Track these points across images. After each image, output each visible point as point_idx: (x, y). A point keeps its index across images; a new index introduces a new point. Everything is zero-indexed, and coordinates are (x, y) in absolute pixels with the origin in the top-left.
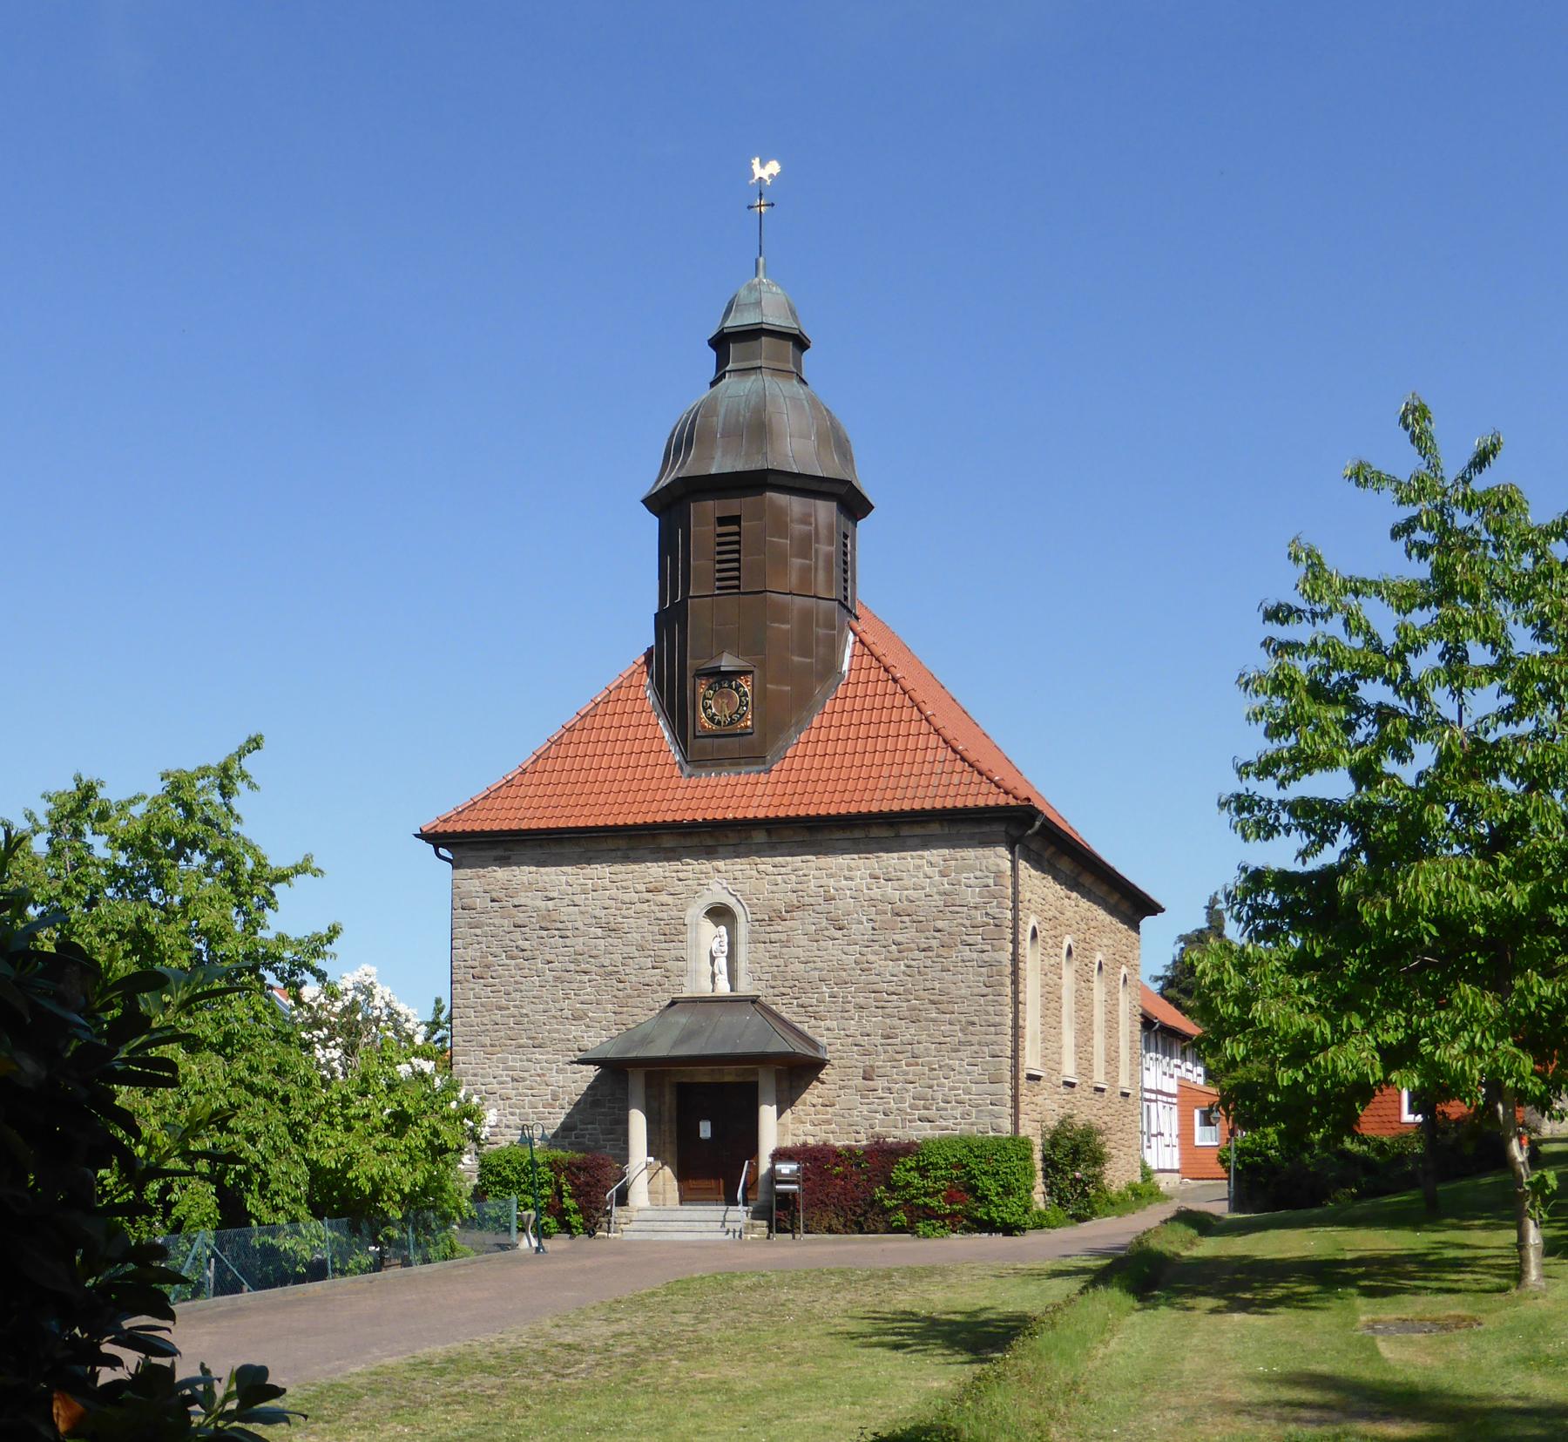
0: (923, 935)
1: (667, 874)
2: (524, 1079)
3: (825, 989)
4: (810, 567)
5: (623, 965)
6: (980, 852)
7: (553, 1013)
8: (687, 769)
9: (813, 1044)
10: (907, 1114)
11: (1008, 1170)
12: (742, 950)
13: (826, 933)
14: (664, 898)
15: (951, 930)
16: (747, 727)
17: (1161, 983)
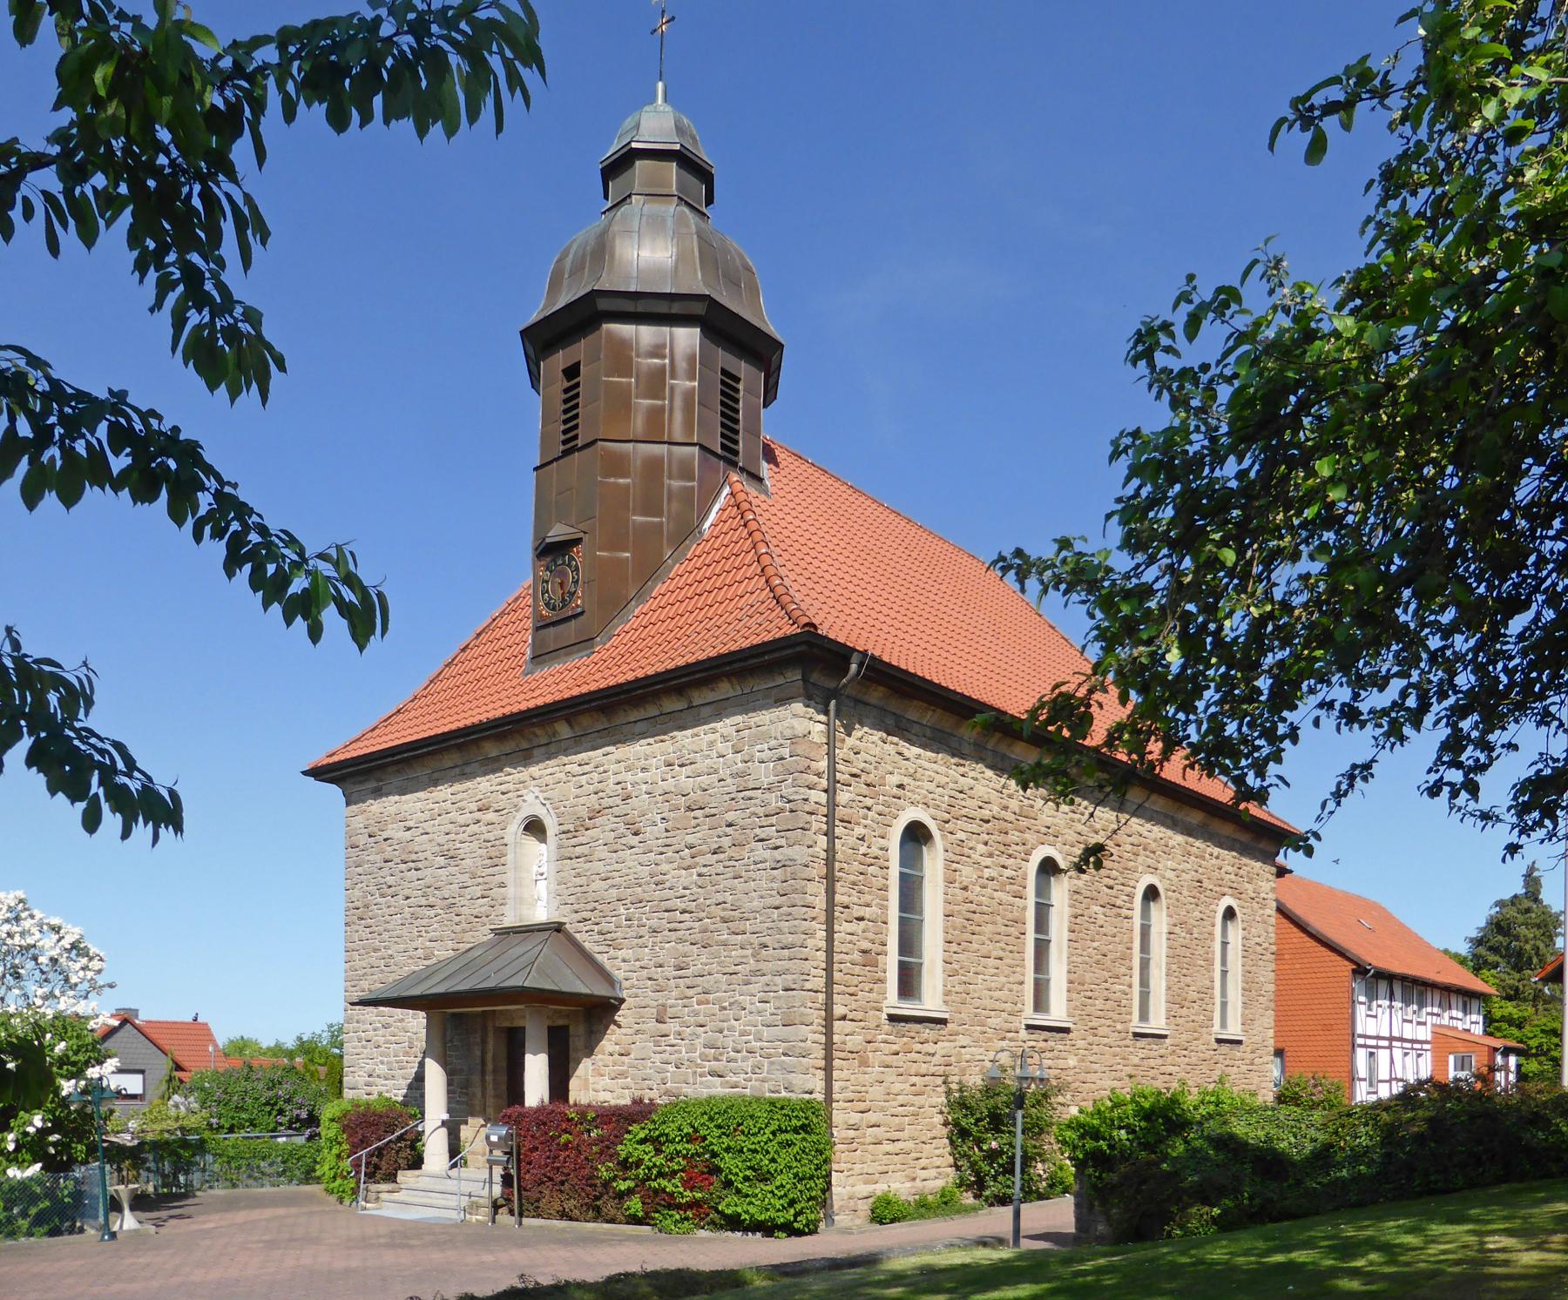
1: (494, 788)
3: (622, 911)
4: (662, 408)
10: (698, 1066)
13: (623, 841)
15: (742, 823)
16: (577, 606)
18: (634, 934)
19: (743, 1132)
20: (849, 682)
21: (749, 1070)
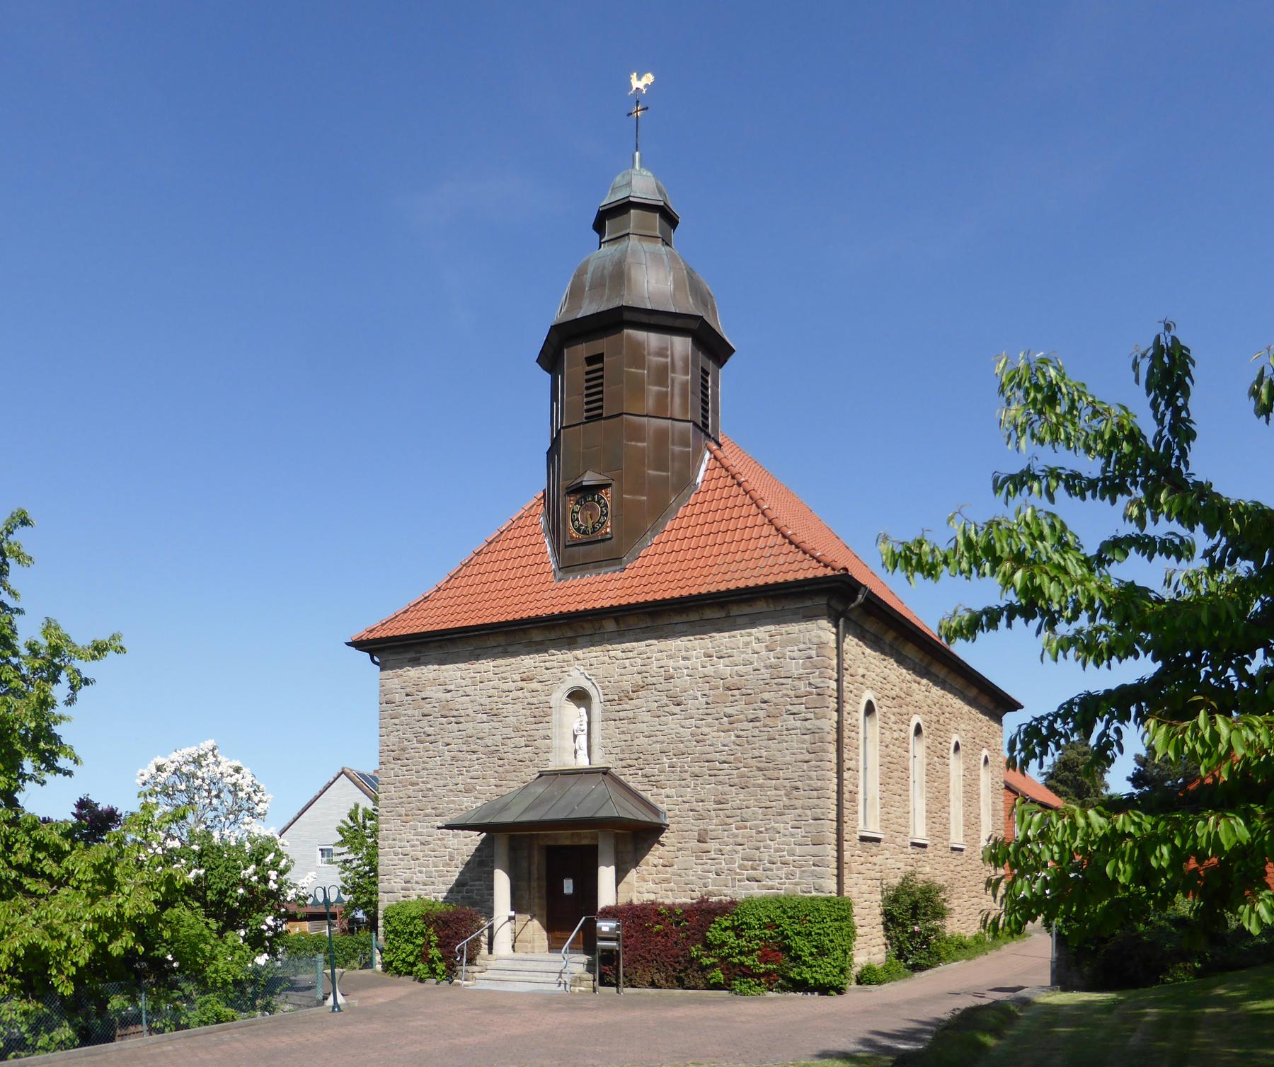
0: (751, 707)
1: (537, 664)
2: (428, 843)
3: (665, 760)
5: (503, 744)
6: (804, 626)
7: (451, 787)
8: (560, 574)
9: (654, 810)
10: (737, 874)
11: (821, 931)
12: (596, 727)
13: (666, 709)
14: (534, 685)
15: (775, 701)
16: (606, 533)
17: (1045, 776)
18: (678, 778)
19: (810, 921)
20: (856, 607)
21: (783, 876)
